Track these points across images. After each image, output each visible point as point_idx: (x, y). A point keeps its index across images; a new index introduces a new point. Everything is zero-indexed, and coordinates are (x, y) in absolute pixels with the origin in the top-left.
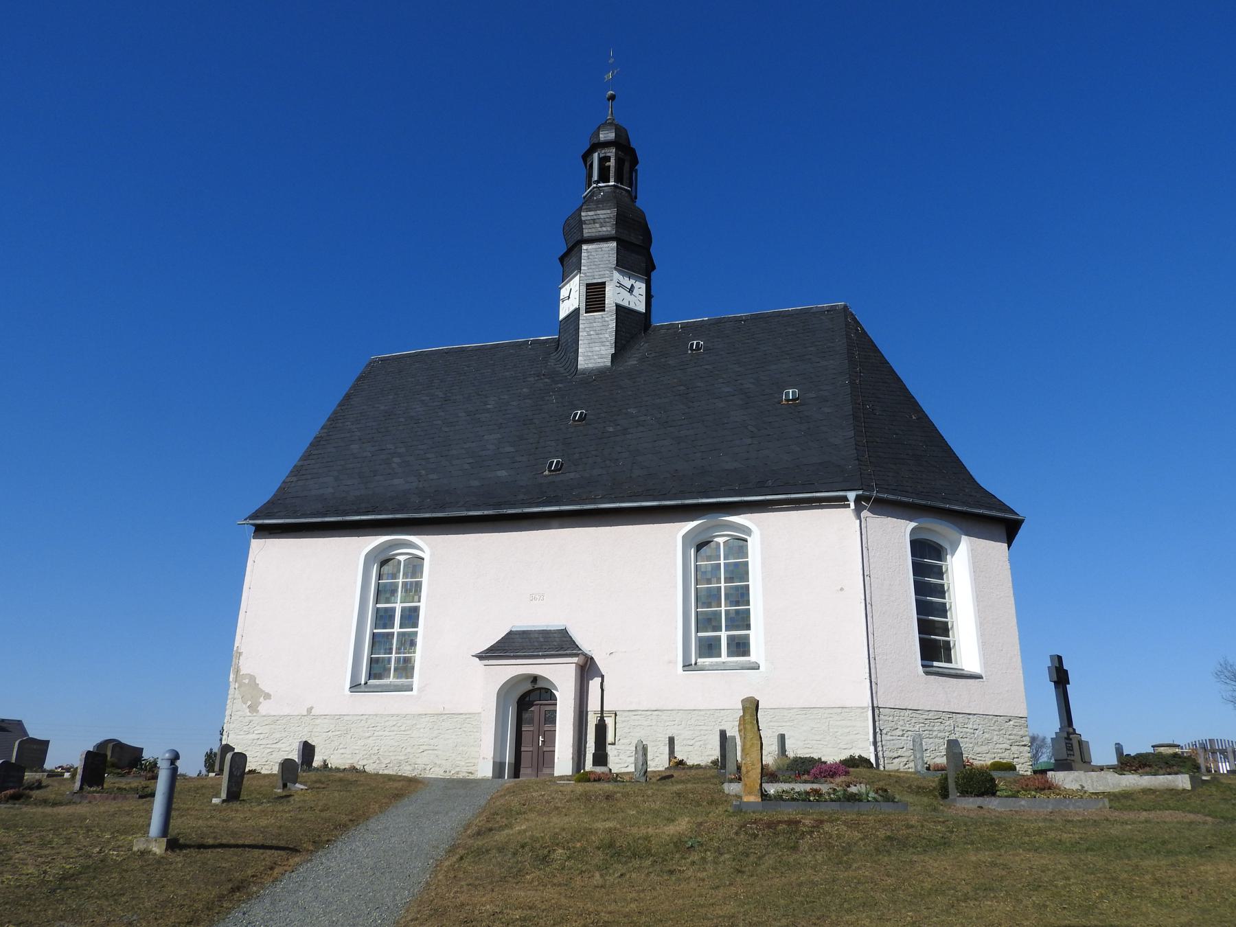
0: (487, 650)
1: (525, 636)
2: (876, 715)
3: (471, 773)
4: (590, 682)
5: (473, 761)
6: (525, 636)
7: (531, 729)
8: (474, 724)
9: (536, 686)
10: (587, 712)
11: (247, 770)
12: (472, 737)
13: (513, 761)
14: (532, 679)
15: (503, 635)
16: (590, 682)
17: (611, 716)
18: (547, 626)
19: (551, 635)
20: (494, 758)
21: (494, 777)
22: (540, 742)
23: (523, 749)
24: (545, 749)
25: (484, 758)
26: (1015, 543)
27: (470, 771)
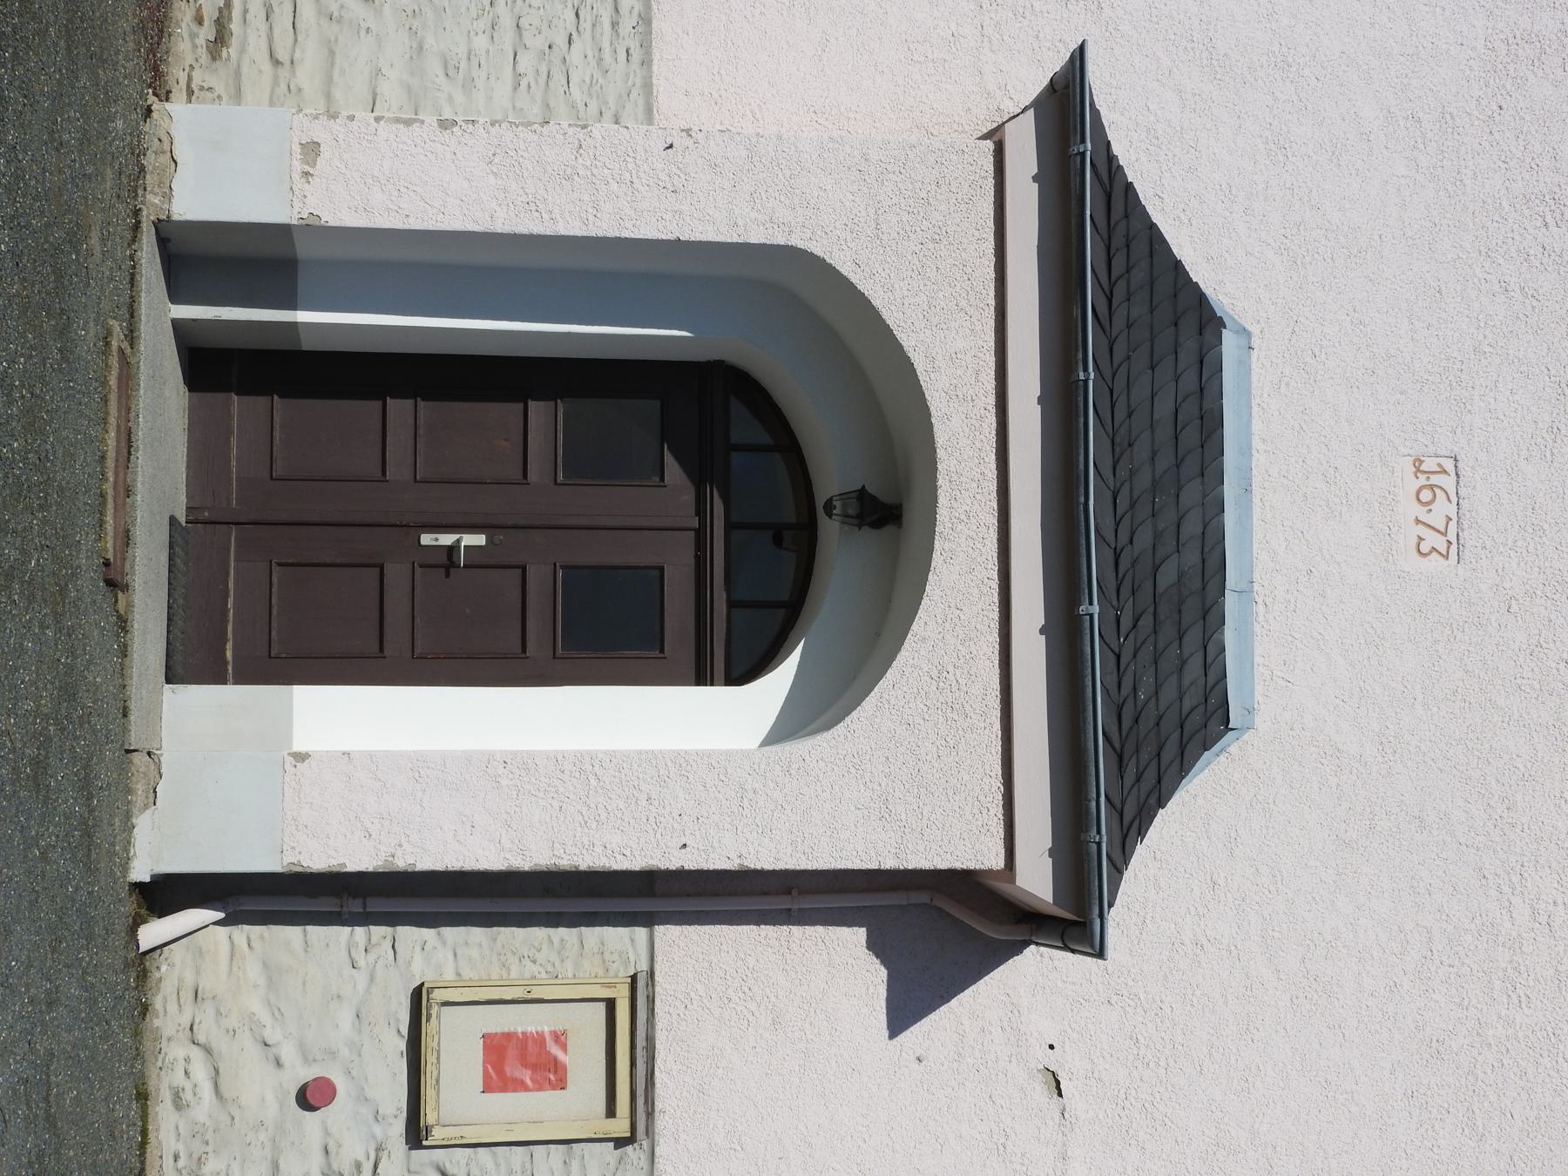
0: (1111, 159)
1: (1190, 437)
2: (462, 1142)
3: (221, 38)
4: (859, 934)
5: (310, 57)
6: (1190, 437)
7: (537, 470)
8: (575, 56)
9: (830, 530)
10: (648, 920)
11: (448, 563)
12: (481, 42)
13: (308, 344)
14: (884, 497)
15: (1200, 273)
16: (859, 934)
17: (611, 1112)
18: (1246, 592)
19: (1193, 638)
20: (316, 231)
21: (139, 887)
22: (447, 539)
23: (399, 409)
24: (396, 573)
25: (311, 150)
26: (915, 1035)
27: (235, 26)
